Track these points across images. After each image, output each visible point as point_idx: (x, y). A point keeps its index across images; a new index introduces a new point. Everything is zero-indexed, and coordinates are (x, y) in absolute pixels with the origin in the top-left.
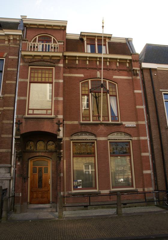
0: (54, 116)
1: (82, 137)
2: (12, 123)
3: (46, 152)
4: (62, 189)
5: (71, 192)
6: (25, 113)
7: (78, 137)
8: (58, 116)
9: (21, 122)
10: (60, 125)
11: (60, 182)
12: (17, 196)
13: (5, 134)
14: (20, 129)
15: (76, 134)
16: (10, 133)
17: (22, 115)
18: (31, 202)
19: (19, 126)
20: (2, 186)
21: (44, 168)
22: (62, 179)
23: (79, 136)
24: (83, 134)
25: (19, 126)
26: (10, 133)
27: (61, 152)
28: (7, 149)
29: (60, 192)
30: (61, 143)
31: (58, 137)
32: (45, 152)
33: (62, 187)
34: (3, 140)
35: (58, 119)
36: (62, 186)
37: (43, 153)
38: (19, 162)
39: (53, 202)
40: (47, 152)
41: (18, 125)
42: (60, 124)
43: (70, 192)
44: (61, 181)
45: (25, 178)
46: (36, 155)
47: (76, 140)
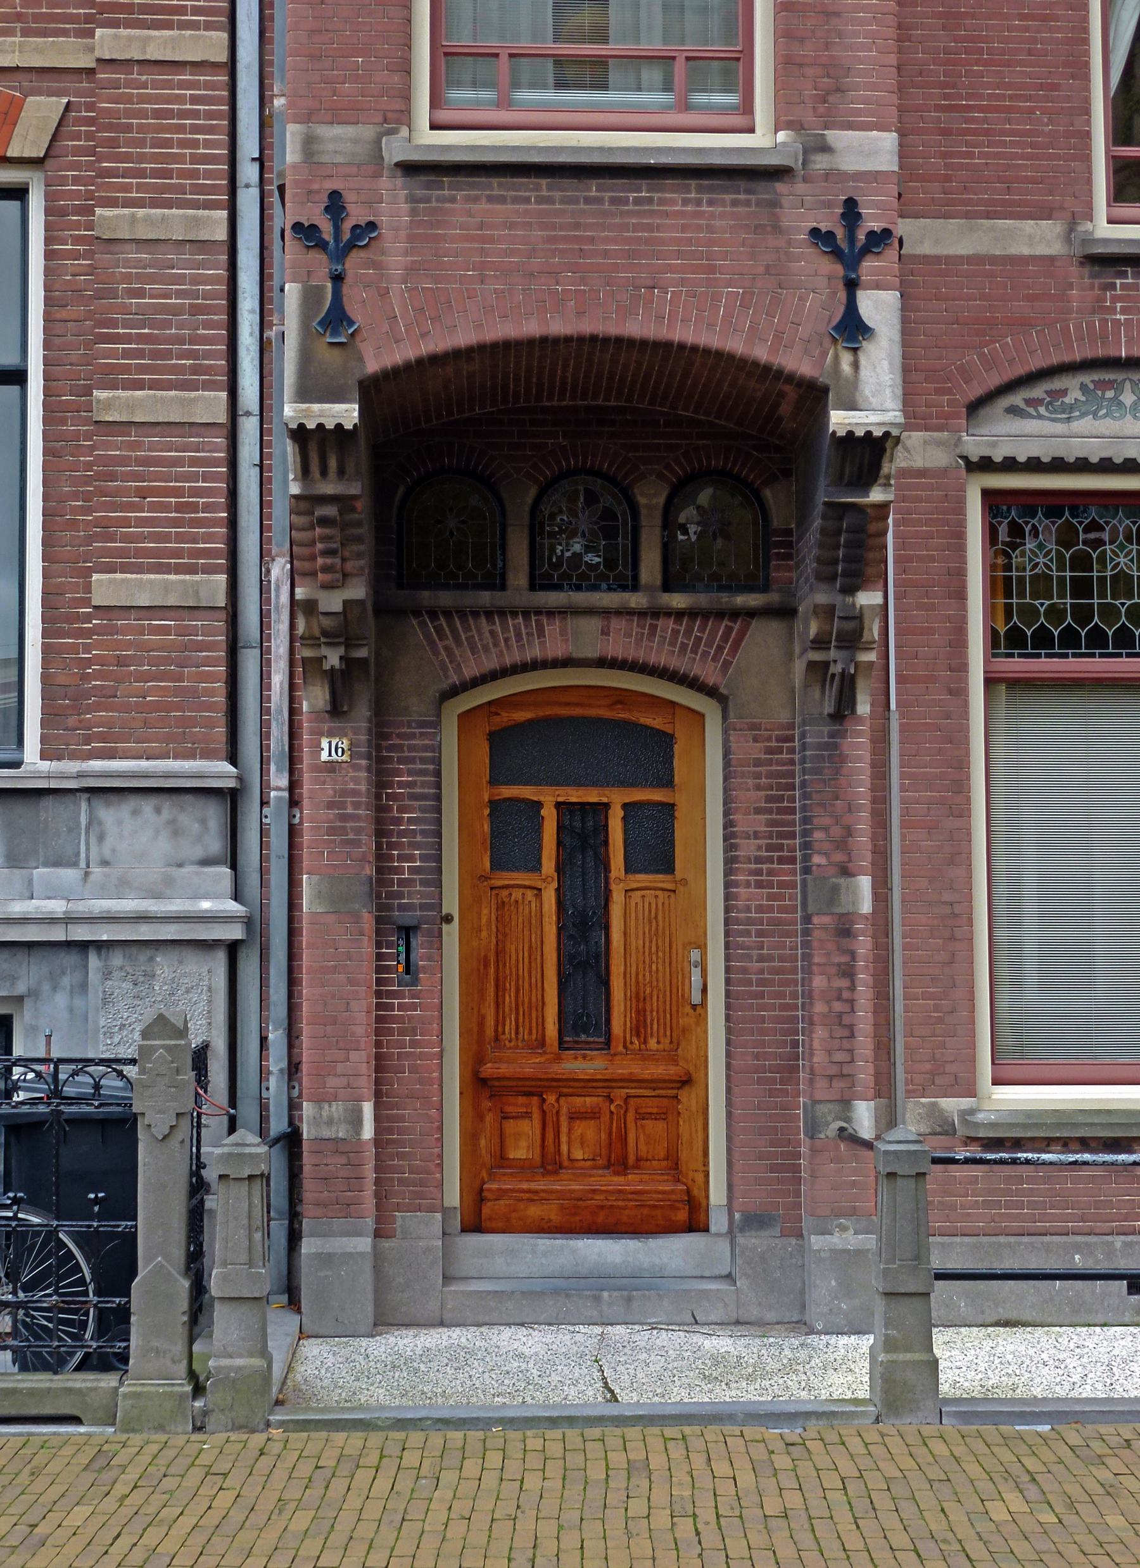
0: (782, 136)
1: (1106, 426)
2: (221, 234)
3: (656, 613)
4: (864, 1073)
5: (966, 1103)
6: (406, 95)
7: (1059, 428)
8: (837, 137)
9: (356, 215)
10: (869, 264)
11: (844, 983)
12: (327, 1133)
13: (139, 385)
14: (353, 309)
15: (1038, 391)
16: (195, 370)
17: (367, 132)
18: (486, 1210)
19: (338, 279)
20: (164, 1011)
21: (628, 807)
22: (863, 946)
23: (1069, 413)
24: (1118, 387)
25: (338, 279)
26: (195, 370)
27: (857, 618)
28: (178, 569)
29: (845, 1103)
30: (877, 495)
31: (839, 420)
32: (642, 614)
33: (864, 1044)
34: (124, 461)
35: (830, 175)
36: (864, 1018)
37: (617, 624)
38: (341, 734)
39: (756, 1221)
40: (668, 613)
41: (321, 265)
42: (866, 250)
43: (952, 1105)
44: (848, 972)
45: (407, 932)
46: (535, 652)
47: (1034, 466)
